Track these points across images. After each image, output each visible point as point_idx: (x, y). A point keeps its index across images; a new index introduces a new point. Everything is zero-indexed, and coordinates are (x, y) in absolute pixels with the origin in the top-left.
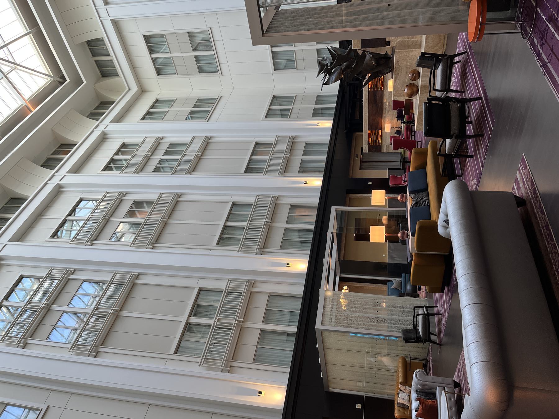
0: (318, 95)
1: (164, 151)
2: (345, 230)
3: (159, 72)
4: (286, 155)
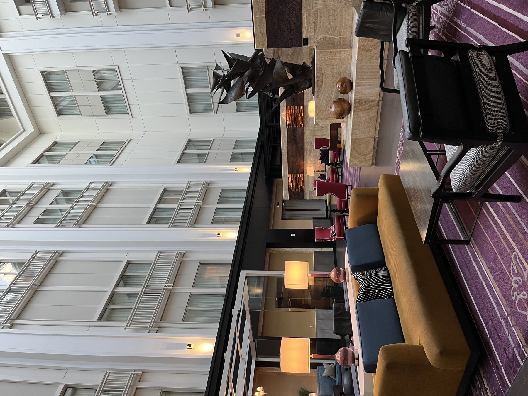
4: (198, 202)
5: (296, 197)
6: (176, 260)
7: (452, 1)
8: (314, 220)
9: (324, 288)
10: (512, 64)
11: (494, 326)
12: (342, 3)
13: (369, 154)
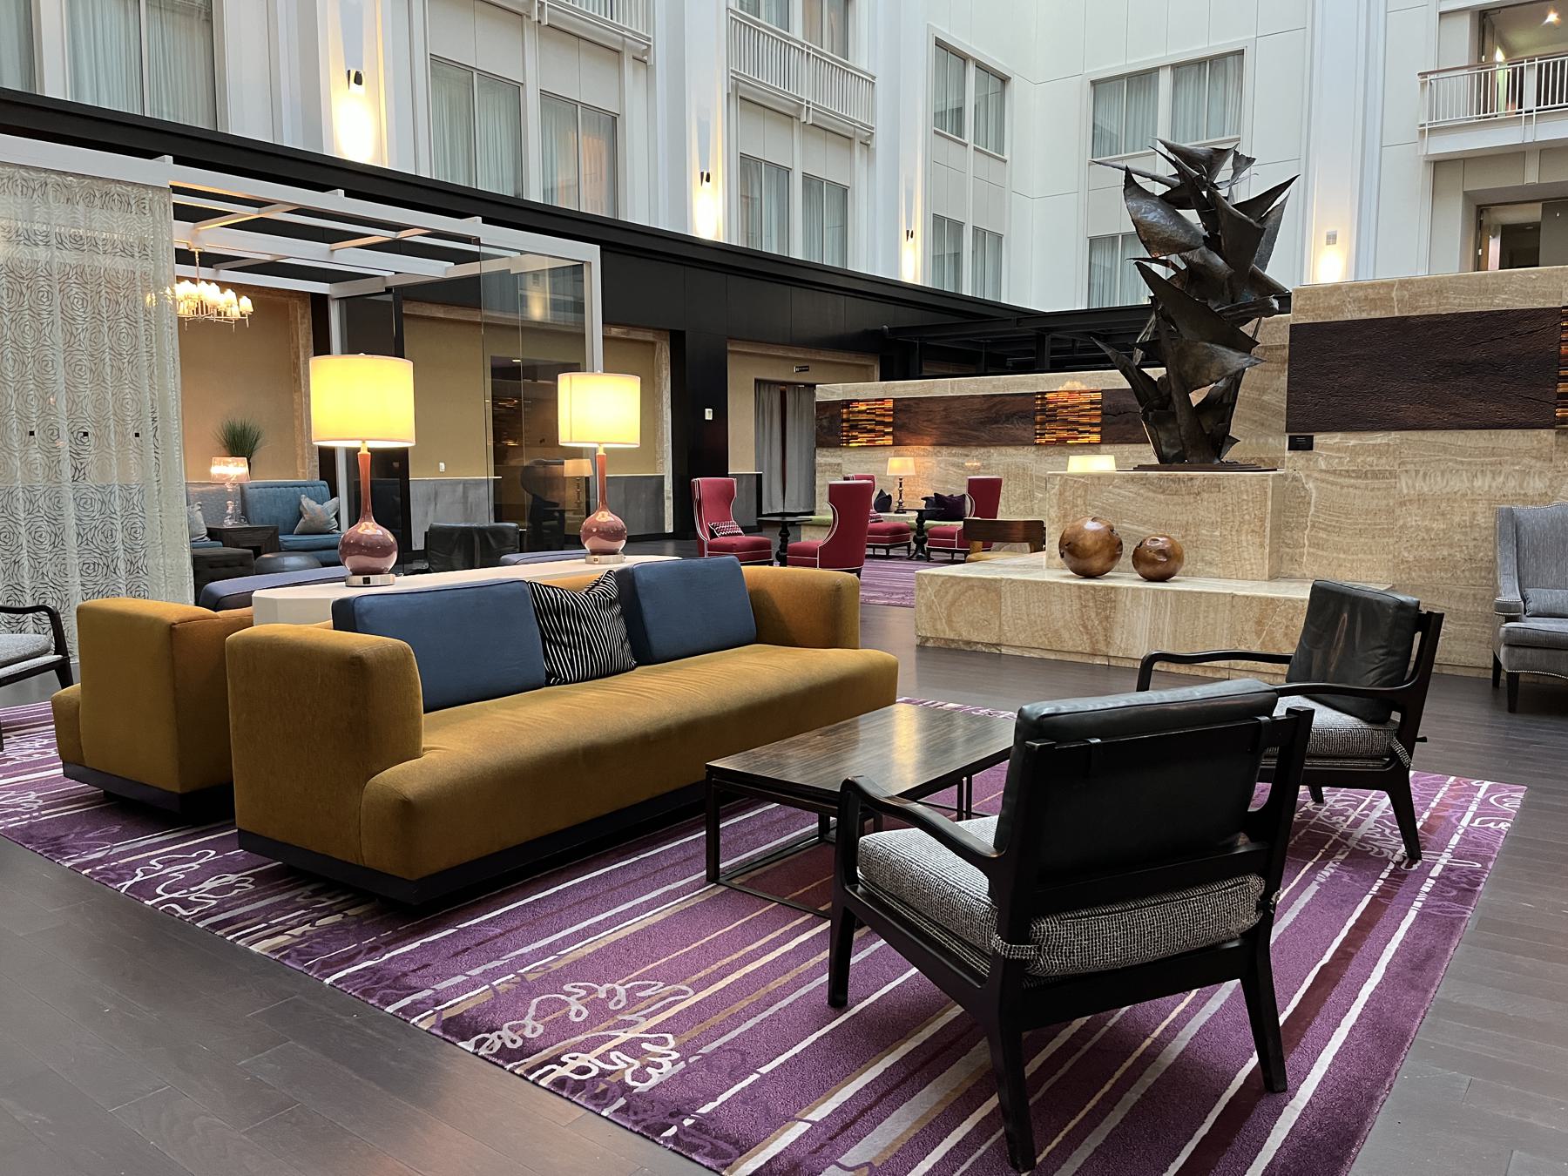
0: (1003, 239)
4: (808, 108)
5: (825, 423)
6: (626, 33)
7: (1393, 847)
8: (755, 479)
9: (556, 505)
10: (1210, 995)
11: (489, 940)
12: (1409, 552)
13: (952, 628)
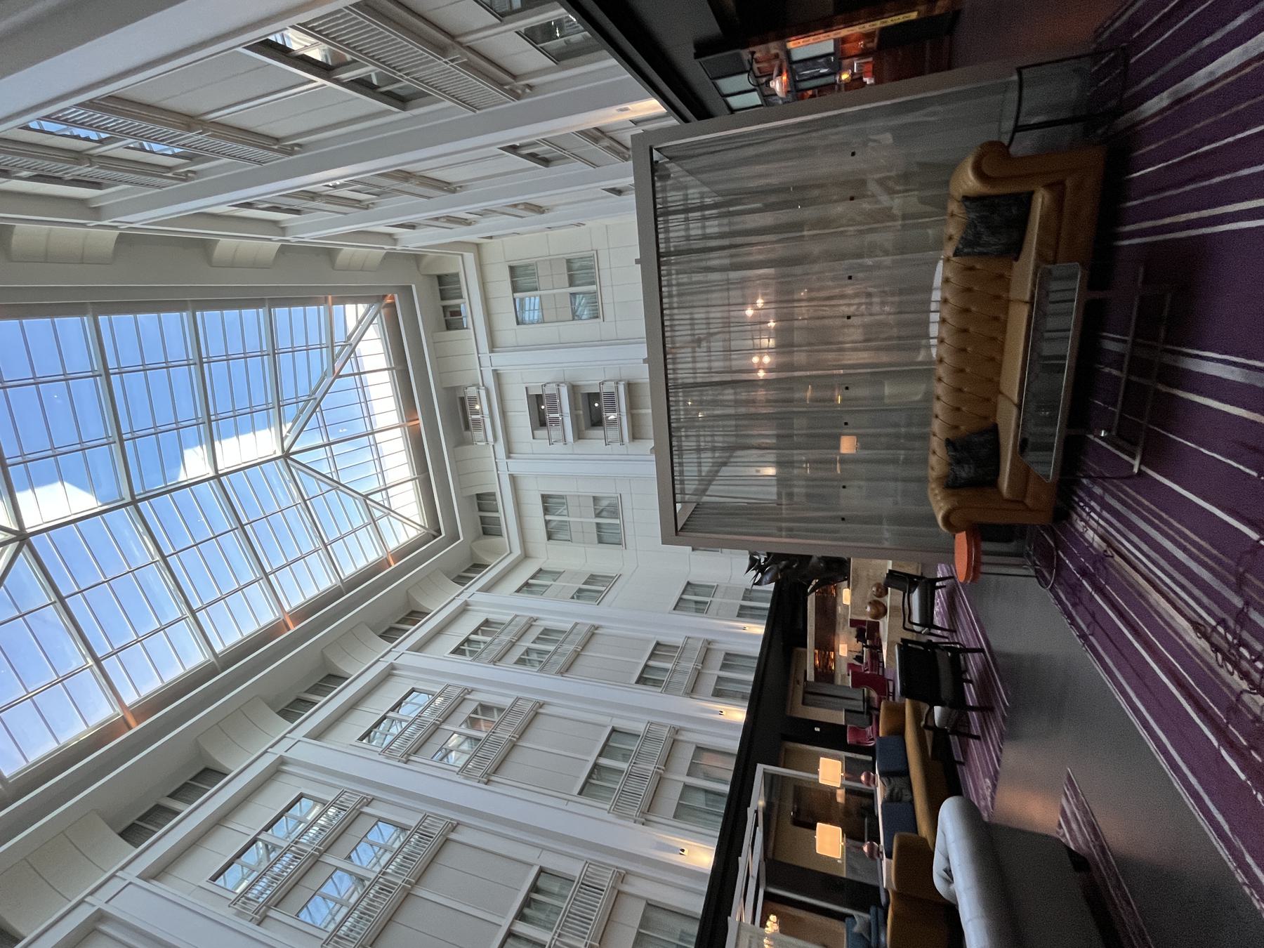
1: (534, 637)
2: (776, 808)
3: (550, 537)
